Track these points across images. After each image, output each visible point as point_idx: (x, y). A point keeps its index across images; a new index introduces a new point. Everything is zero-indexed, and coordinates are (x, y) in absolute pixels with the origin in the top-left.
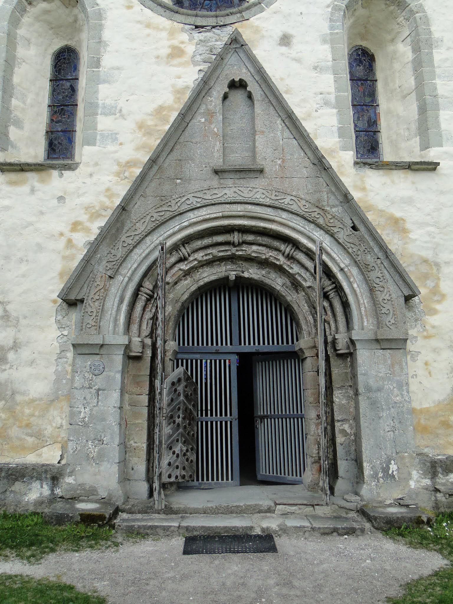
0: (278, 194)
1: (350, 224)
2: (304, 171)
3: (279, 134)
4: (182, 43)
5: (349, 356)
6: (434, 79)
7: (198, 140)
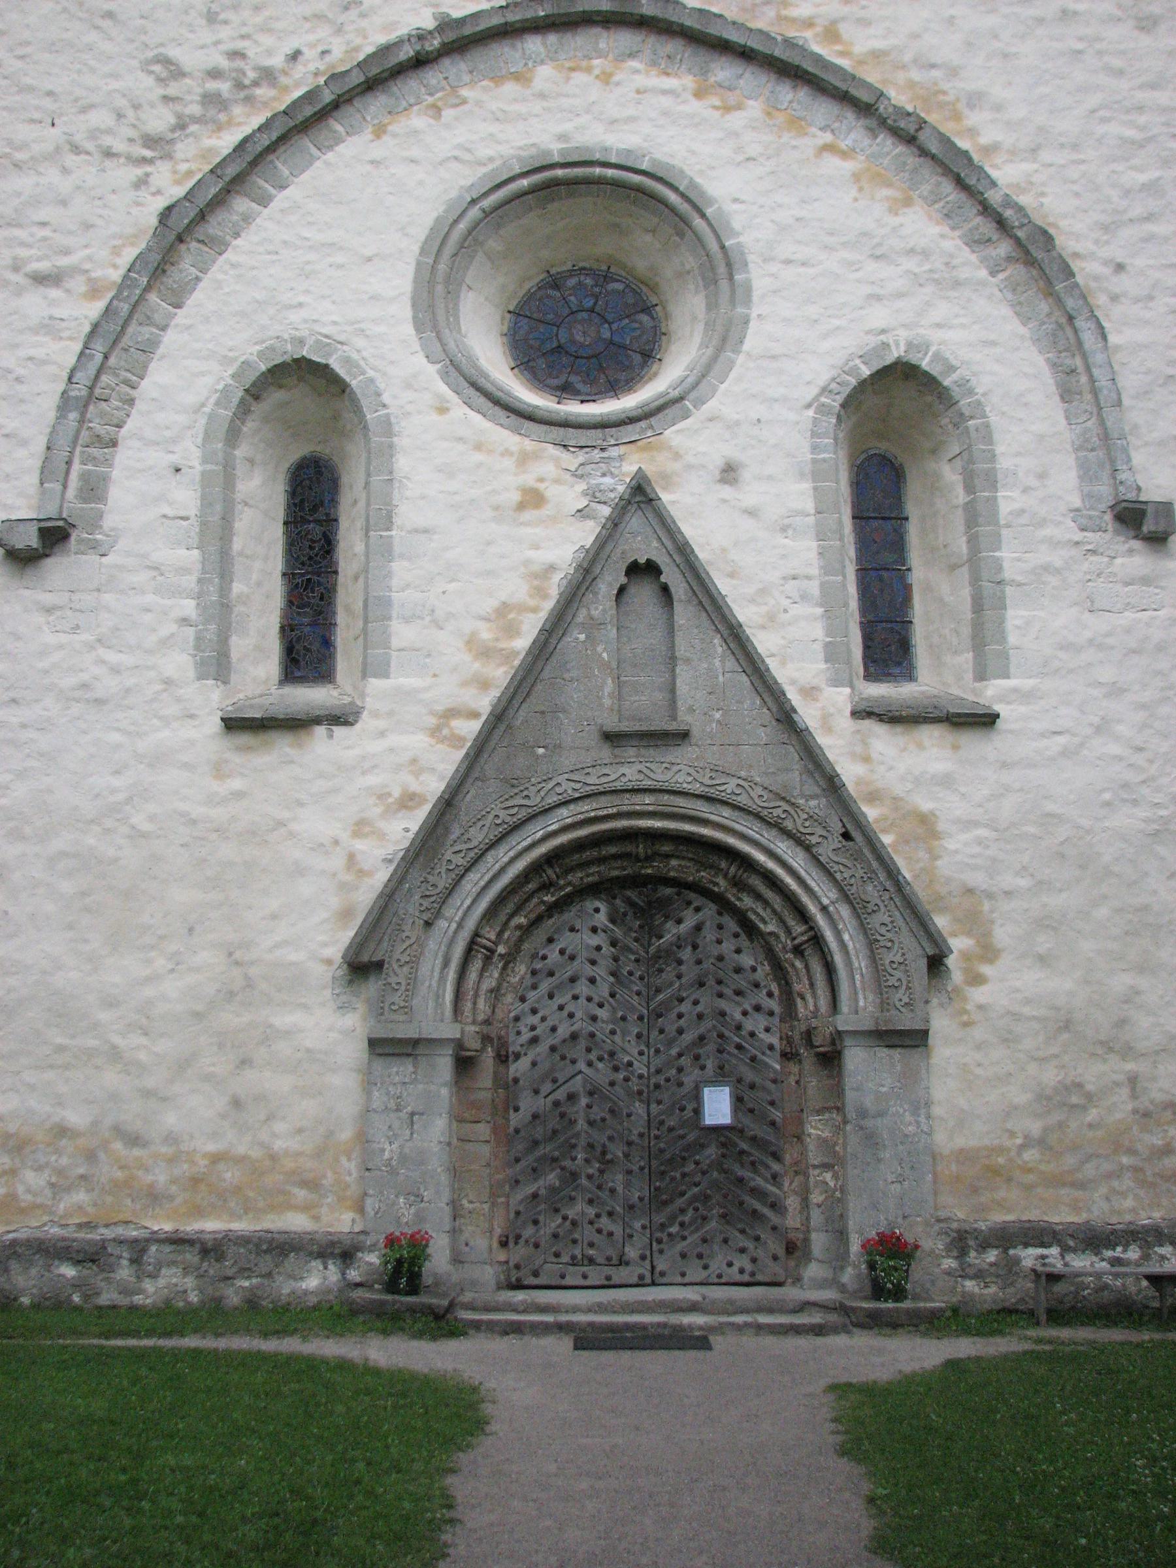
0: (716, 768)
1: (838, 828)
2: (761, 732)
3: (717, 662)
4: (541, 480)
5: (831, 1059)
6: (999, 549)
7: (574, 673)
